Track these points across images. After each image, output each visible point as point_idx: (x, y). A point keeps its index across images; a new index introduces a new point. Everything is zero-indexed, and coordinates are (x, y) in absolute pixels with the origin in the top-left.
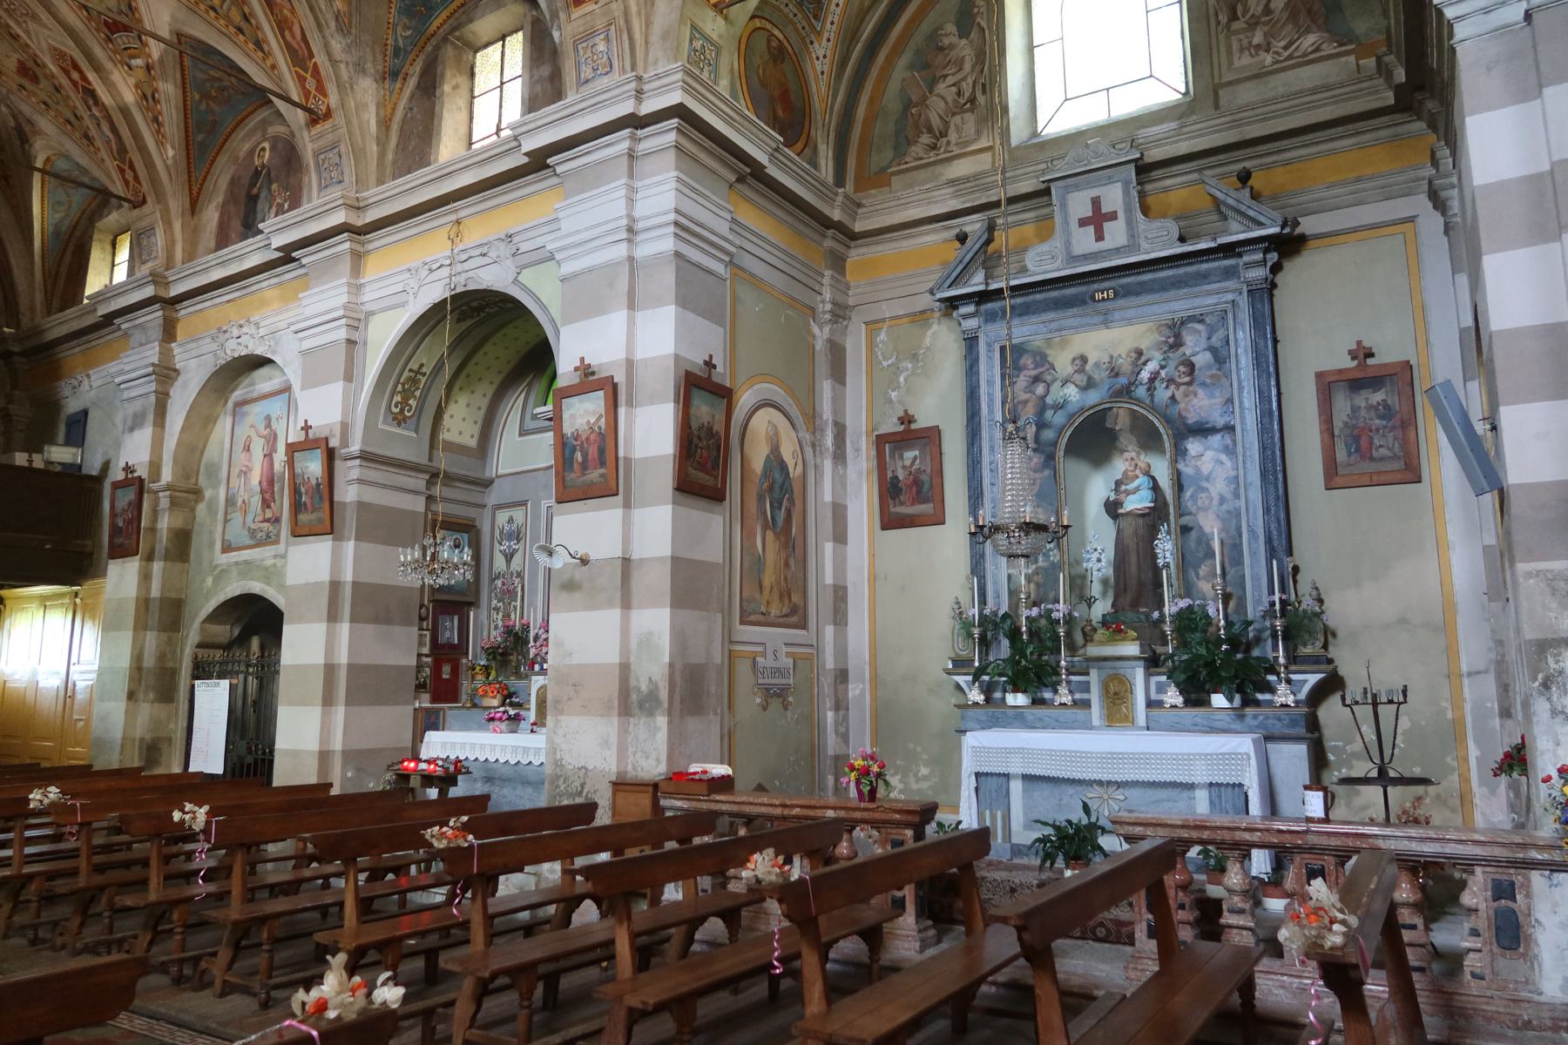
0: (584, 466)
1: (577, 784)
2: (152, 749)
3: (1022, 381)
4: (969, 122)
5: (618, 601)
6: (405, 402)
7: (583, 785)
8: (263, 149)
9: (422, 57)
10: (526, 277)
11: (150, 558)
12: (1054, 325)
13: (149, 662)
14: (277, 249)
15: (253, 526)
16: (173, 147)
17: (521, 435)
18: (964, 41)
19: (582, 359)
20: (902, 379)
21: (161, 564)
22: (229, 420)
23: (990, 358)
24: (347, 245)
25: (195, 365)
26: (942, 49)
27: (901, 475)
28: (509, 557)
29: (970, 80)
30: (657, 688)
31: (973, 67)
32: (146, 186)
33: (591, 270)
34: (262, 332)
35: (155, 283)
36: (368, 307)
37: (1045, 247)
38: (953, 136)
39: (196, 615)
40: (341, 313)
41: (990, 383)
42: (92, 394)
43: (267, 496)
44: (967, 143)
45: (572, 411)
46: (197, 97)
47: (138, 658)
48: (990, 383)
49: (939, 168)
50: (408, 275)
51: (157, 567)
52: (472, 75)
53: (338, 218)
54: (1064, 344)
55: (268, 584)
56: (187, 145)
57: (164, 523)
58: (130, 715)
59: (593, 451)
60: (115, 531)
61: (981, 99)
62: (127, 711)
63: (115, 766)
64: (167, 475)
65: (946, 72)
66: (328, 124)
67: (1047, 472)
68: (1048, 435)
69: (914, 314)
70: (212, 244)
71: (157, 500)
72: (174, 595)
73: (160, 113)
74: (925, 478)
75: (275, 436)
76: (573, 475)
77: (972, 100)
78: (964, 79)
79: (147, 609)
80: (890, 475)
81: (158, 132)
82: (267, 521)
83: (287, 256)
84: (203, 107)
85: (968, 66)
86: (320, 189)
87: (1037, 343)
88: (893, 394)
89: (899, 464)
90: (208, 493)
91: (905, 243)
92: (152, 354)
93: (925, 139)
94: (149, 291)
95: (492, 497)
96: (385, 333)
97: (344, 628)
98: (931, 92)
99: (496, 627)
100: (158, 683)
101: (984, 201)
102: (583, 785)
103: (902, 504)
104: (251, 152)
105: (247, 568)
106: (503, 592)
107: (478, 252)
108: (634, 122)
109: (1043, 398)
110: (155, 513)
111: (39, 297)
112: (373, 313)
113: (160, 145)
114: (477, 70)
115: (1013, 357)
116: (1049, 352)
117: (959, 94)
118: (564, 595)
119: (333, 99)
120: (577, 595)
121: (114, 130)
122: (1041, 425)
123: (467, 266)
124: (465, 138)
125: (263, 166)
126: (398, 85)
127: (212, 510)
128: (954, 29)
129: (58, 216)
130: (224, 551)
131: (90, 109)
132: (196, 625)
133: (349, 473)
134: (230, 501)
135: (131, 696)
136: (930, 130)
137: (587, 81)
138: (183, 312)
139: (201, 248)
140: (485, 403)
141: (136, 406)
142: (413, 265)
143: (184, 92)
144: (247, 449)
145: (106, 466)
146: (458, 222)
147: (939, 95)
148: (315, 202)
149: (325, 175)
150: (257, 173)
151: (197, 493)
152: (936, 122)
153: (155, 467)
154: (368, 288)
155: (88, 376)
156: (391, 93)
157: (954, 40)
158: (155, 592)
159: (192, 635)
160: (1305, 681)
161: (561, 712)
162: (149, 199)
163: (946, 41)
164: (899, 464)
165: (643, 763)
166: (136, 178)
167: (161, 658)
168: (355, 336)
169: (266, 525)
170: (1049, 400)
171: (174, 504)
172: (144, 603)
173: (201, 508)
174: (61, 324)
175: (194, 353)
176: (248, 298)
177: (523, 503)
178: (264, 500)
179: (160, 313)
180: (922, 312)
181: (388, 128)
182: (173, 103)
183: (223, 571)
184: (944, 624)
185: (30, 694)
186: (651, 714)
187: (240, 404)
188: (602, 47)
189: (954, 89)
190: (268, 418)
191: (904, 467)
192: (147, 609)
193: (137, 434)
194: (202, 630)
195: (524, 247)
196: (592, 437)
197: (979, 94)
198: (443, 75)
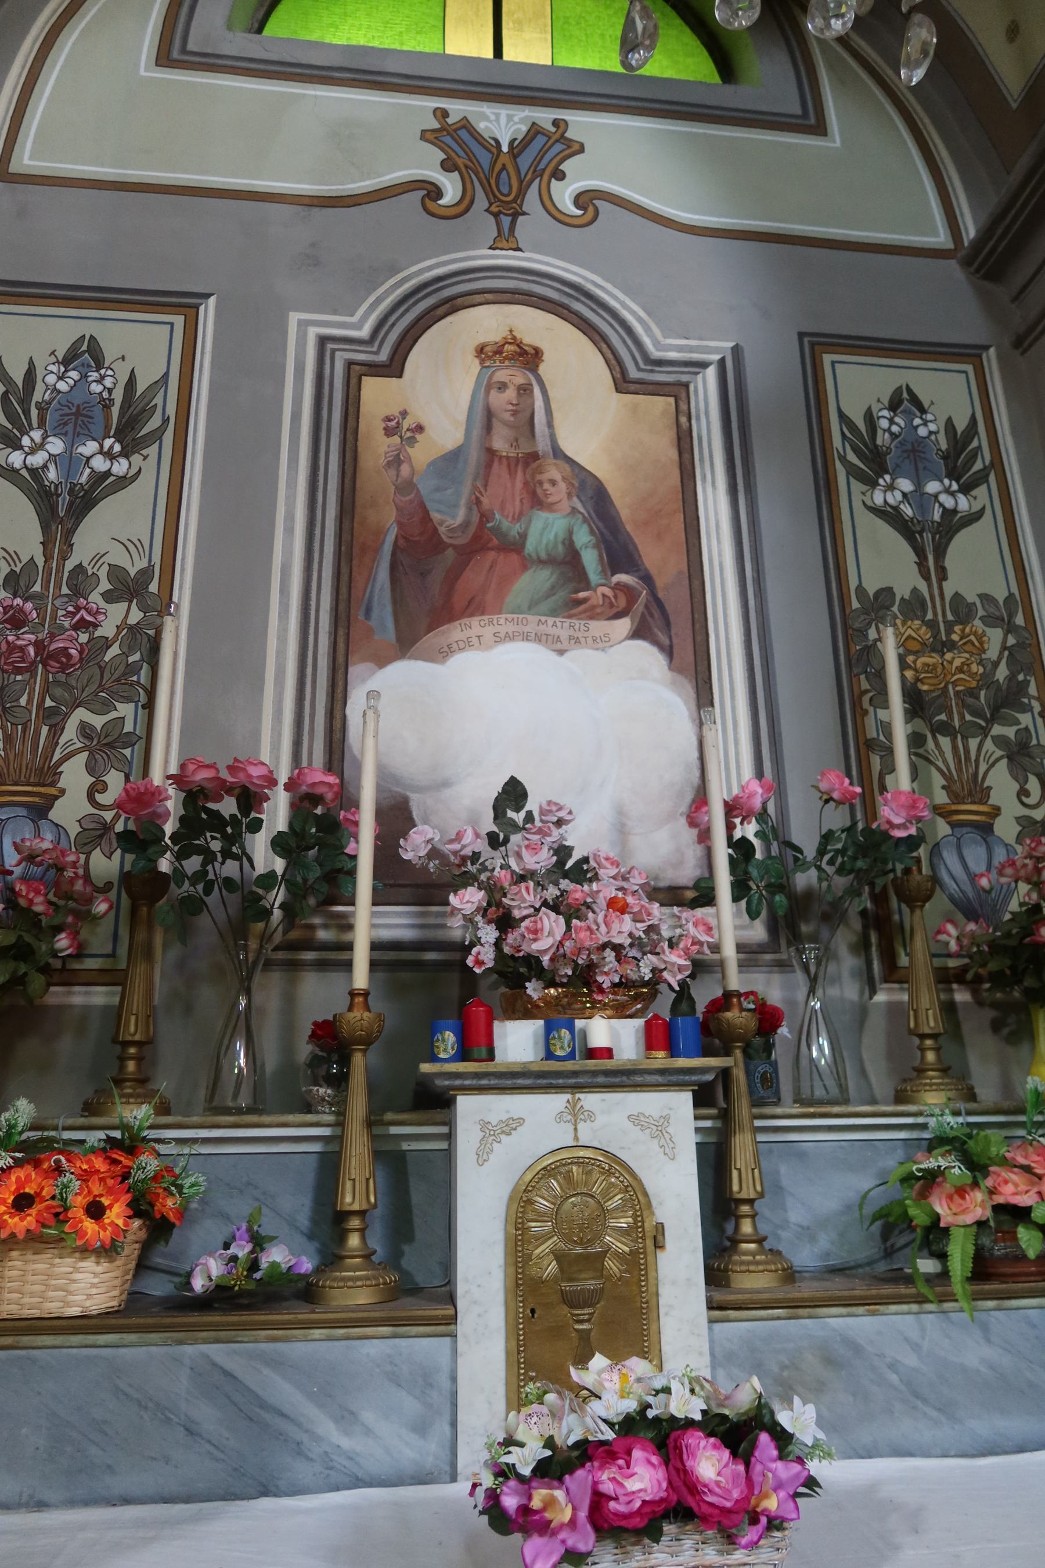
17: (164, 58)
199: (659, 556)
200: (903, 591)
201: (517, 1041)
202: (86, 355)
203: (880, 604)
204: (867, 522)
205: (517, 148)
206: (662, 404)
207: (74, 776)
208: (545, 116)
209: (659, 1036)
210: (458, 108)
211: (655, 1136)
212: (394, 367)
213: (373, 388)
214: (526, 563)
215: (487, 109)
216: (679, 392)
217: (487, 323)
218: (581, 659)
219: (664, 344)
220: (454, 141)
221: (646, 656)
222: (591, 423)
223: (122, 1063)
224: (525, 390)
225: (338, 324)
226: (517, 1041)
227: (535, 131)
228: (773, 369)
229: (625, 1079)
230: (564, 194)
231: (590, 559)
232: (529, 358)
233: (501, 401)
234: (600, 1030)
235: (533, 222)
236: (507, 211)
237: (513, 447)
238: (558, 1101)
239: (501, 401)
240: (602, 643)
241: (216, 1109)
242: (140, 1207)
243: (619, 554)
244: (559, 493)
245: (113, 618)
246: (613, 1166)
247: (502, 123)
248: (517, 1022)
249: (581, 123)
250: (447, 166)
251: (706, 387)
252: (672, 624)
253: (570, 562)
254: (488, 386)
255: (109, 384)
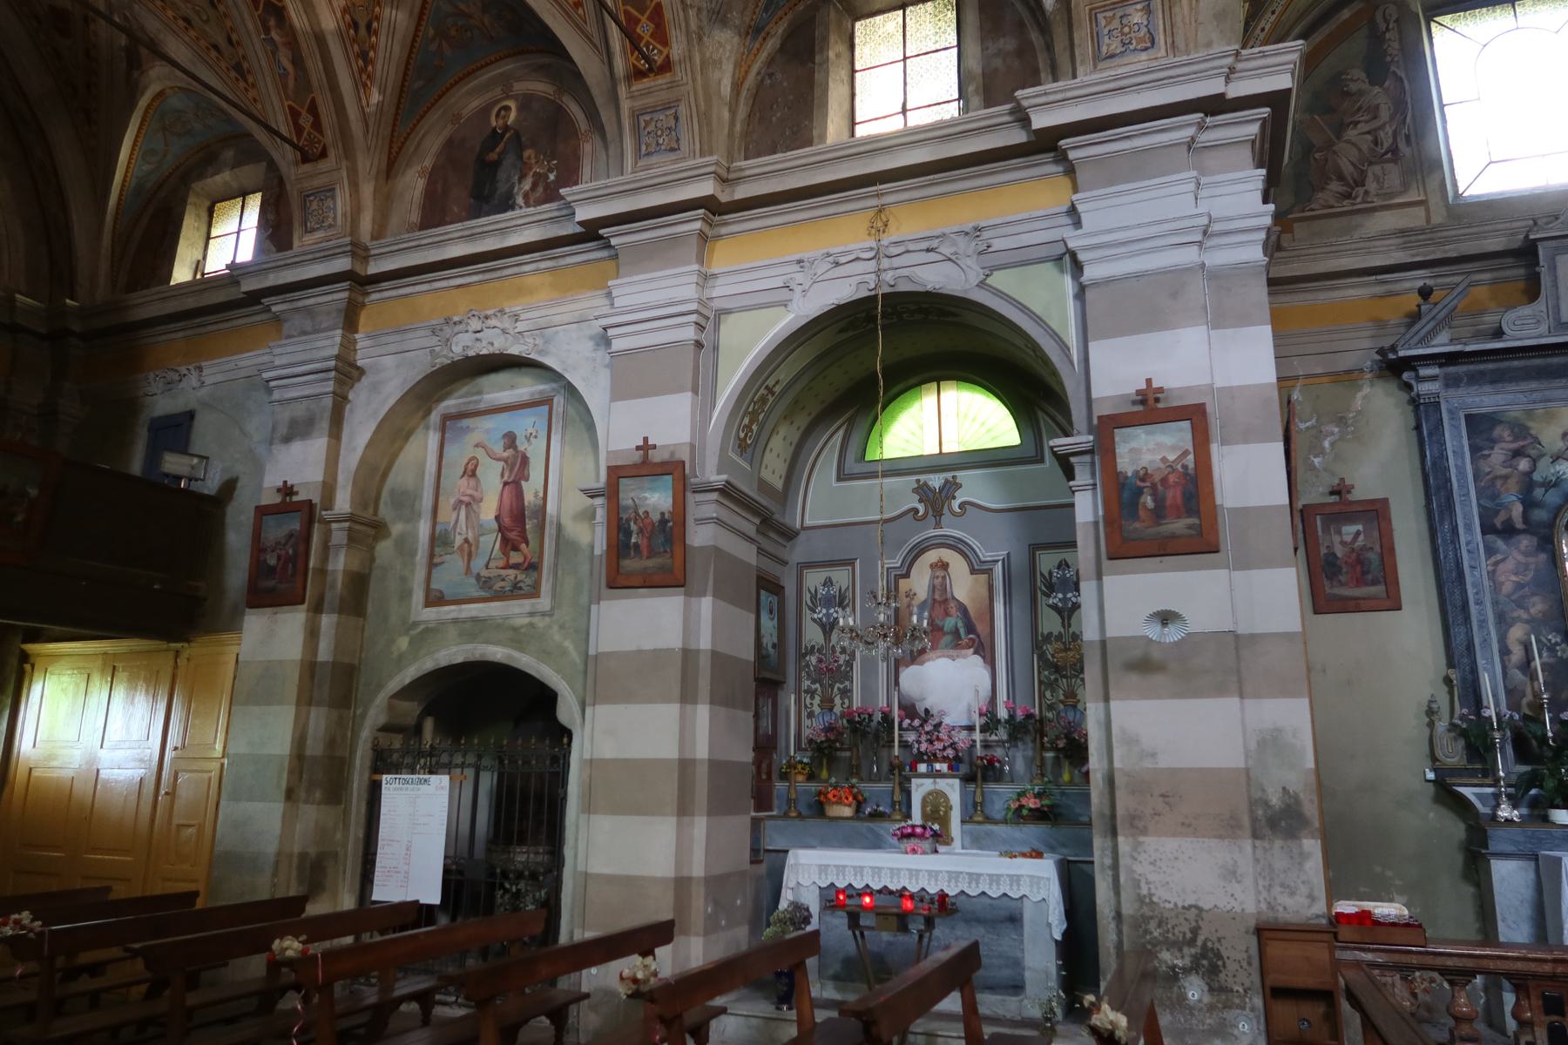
0: (1159, 513)
1: (1186, 928)
2: (315, 871)
3: (1497, 456)
4: (1393, 176)
5: (676, 691)
6: (751, 422)
7: (1195, 931)
8: (507, 109)
9: (790, 16)
10: (999, 280)
11: (317, 609)
12: (1535, 396)
13: (315, 748)
14: (580, 223)
15: (484, 573)
16: (382, 91)
17: (839, 479)
18: (1377, 89)
19: (1149, 381)
20: (1326, 444)
21: (334, 617)
22: (433, 439)
23: (1456, 427)
24: (698, 225)
25: (391, 369)
26: (1348, 94)
27: (1339, 551)
28: (828, 627)
29: (1389, 130)
30: (1297, 801)
31: (1392, 118)
32: (329, 136)
33: (1138, 276)
34: (521, 326)
35: (354, 255)
36: (717, 304)
37: (1526, 310)
38: (1371, 186)
39: (380, 686)
40: (694, 306)
41: (1459, 454)
42: (203, 392)
43: (513, 535)
44: (1392, 195)
45: (1134, 444)
46: (431, 32)
47: (300, 741)
48: (1459, 454)
49: (1357, 219)
50: (797, 268)
51: (327, 621)
52: (852, 47)
53: (705, 188)
54: (1550, 417)
55: (522, 650)
56: (402, 91)
57: (339, 564)
58: (288, 821)
59: (1173, 496)
60: (259, 570)
61: (1405, 150)
62: (284, 816)
63: (264, 895)
64: (343, 502)
65: (1356, 118)
66: (662, 80)
67: (1543, 557)
68: (1540, 515)
69: (1337, 374)
70: (415, 217)
71: (327, 536)
72: (346, 660)
73: (373, 47)
74: (1373, 557)
75: (525, 460)
76: (1137, 525)
77: (1394, 150)
78: (1382, 127)
79: (312, 677)
80: (1323, 551)
81: (362, 71)
82: (516, 566)
83: (591, 232)
84: (433, 47)
85: (1384, 114)
86: (638, 155)
87: (1513, 414)
88: (1317, 461)
89: (1336, 539)
90: (397, 529)
91: (1322, 296)
92: (328, 345)
93: (1335, 186)
94: (342, 264)
95: (798, 552)
96: (749, 342)
97: (703, 712)
98: (1339, 137)
99: (811, 715)
100: (335, 782)
101: (1438, 256)
102: (1195, 931)
103: (1341, 584)
104: (485, 111)
105: (475, 630)
106: (819, 670)
107: (925, 245)
108: (1214, 106)
109: (1528, 474)
110: (326, 547)
111: (104, 266)
112: (728, 312)
113: (361, 86)
114: (857, 41)
115: (1481, 427)
116: (1530, 424)
117: (1376, 143)
118: (1134, 678)
119: (677, 50)
120: (1158, 679)
121: (298, 61)
122: (1529, 504)
123: (897, 262)
124: (847, 115)
125: (506, 128)
126: (757, 45)
127: (405, 547)
128: (1363, 75)
129: (146, 168)
130: (429, 603)
131: (267, 30)
132: (382, 699)
133: (703, 507)
134: (439, 540)
135: (290, 795)
136: (1341, 178)
137: (1112, 56)
138: (374, 296)
139: (394, 221)
140: (796, 438)
141: (299, 410)
142: (805, 256)
143: (419, 24)
144: (471, 472)
145: (229, 487)
146: (881, 210)
147: (1349, 142)
148: (628, 177)
149: (645, 139)
150: (495, 137)
151: (379, 529)
152: (1348, 169)
153: (329, 488)
154: (720, 281)
155: (200, 369)
156: (749, 52)
157: (1366, 86)
158: (324, 653)
159: (375, 714)
160: (1476, 795)
161: (1144, 831)
162: (332, 153)
163: (1353, 87)
164: (1336, 539)
165: (1285, 900)
166: (317, 125)
167: (331, 743)
168: (703, 337)
169: (511, 572)
170: (1536, 477)
171: (353, 539)
172: (310, 668)
173: (384, 548)
174: (147, 306)
175: (393, 348)
176: (497, 284)
177: (850, 562)
178: (505, 541)
179: (345, 295)
180: (1348, 372)
181: (738, 94)
182: (398, 37)
183: (427, 630)
184: (1411, 726)
185: (82, 789)
186: (1292, 834)
187: (447, 418)
188: (1137, 18)
189: (1369, 137)
190: (510, 440)
191: (1343, 543)
192: (312, 677)
193: (297, 447)
194: (391, 708)
195: (997, 244)
196: (1172, 479)
197: (1402, 145)
198: (825, 39)
199: (981, 628)
200: (1055, 633)
201: (922, 768)
202: (828, 582)
203: (1048, 638)
204: (1047, 610)
205: (941, 489)
206: (984, 577)
207: (838, 701)
208: (949, 475)
209: (950, 768)
210: (922, 478)
211: (952, 789)
212: (907, 575)
213: (902, 582)
214: (945, 634)
215: (931, 476)
216: (989, 572)
217: (932, 556)
218: (960, 662)
219: (985, 555)
220: (922, 491)
221: (977, 659)
222: (963, 587)
223: (854, 770)
224: (944, 578)
225: (889, 563)
226: (922, 768)
227: (947, 482)
228: (1020, 562)
229: (943, 776)
230: (955, 505)
231: (962, 631)
232: (944, 566)
233: (937, 582)
234: (938, 766)
235: (947, 518)
236: (938, 514)
237: (940, 599)
238: (931, 780)
239: (937, 582)
240: (965, 657)
241: (870, 780)
242: (855, 798)
243: (970, 628)
244: (953, 611)
245: (842, 658)
246: (945, 796)
247: (936, 481)
248: (1204, 701)
249: (962, 476)
250: (920, 501)
251: (998, 568)
252: (985, 650)
253: (956, 633)
254: (934, 577)
255: (834, 591)
